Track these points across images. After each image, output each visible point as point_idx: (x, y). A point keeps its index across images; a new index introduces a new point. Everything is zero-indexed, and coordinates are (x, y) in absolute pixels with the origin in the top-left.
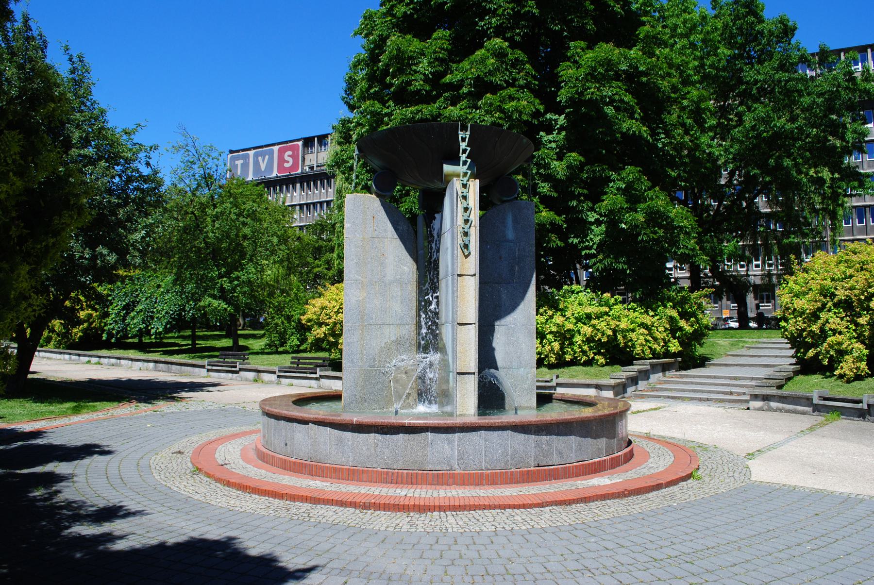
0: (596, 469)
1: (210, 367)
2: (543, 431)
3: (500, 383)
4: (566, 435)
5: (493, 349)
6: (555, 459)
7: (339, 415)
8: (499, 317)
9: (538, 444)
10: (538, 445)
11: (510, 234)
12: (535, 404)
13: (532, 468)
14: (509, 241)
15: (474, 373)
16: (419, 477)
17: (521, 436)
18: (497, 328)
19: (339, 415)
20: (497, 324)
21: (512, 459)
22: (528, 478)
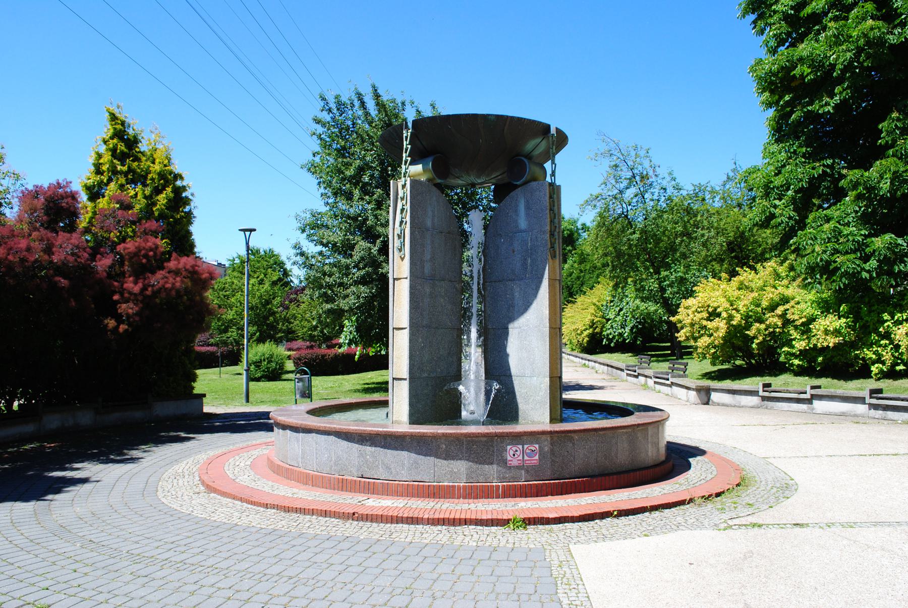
0: (487, 493)
1: (766, 394)
2: (367, 441)
3: (770, 398)
4: (396, 449)
5: (508, 355)
6: (381, 473)
7: (386, 426)
8: (512, 319)
9: (361, 454)
10: (361, 455)
11: (523, 223)
12: (548, 420)
13: (355, 478)
14: (521, 231)
15: (405, 379)
16: (362, 485)
17: (345, 444)
18: (510, 330)
19: (386, 426)
20: (511, 326)
21: (336, 465)
22: (344, 485)
